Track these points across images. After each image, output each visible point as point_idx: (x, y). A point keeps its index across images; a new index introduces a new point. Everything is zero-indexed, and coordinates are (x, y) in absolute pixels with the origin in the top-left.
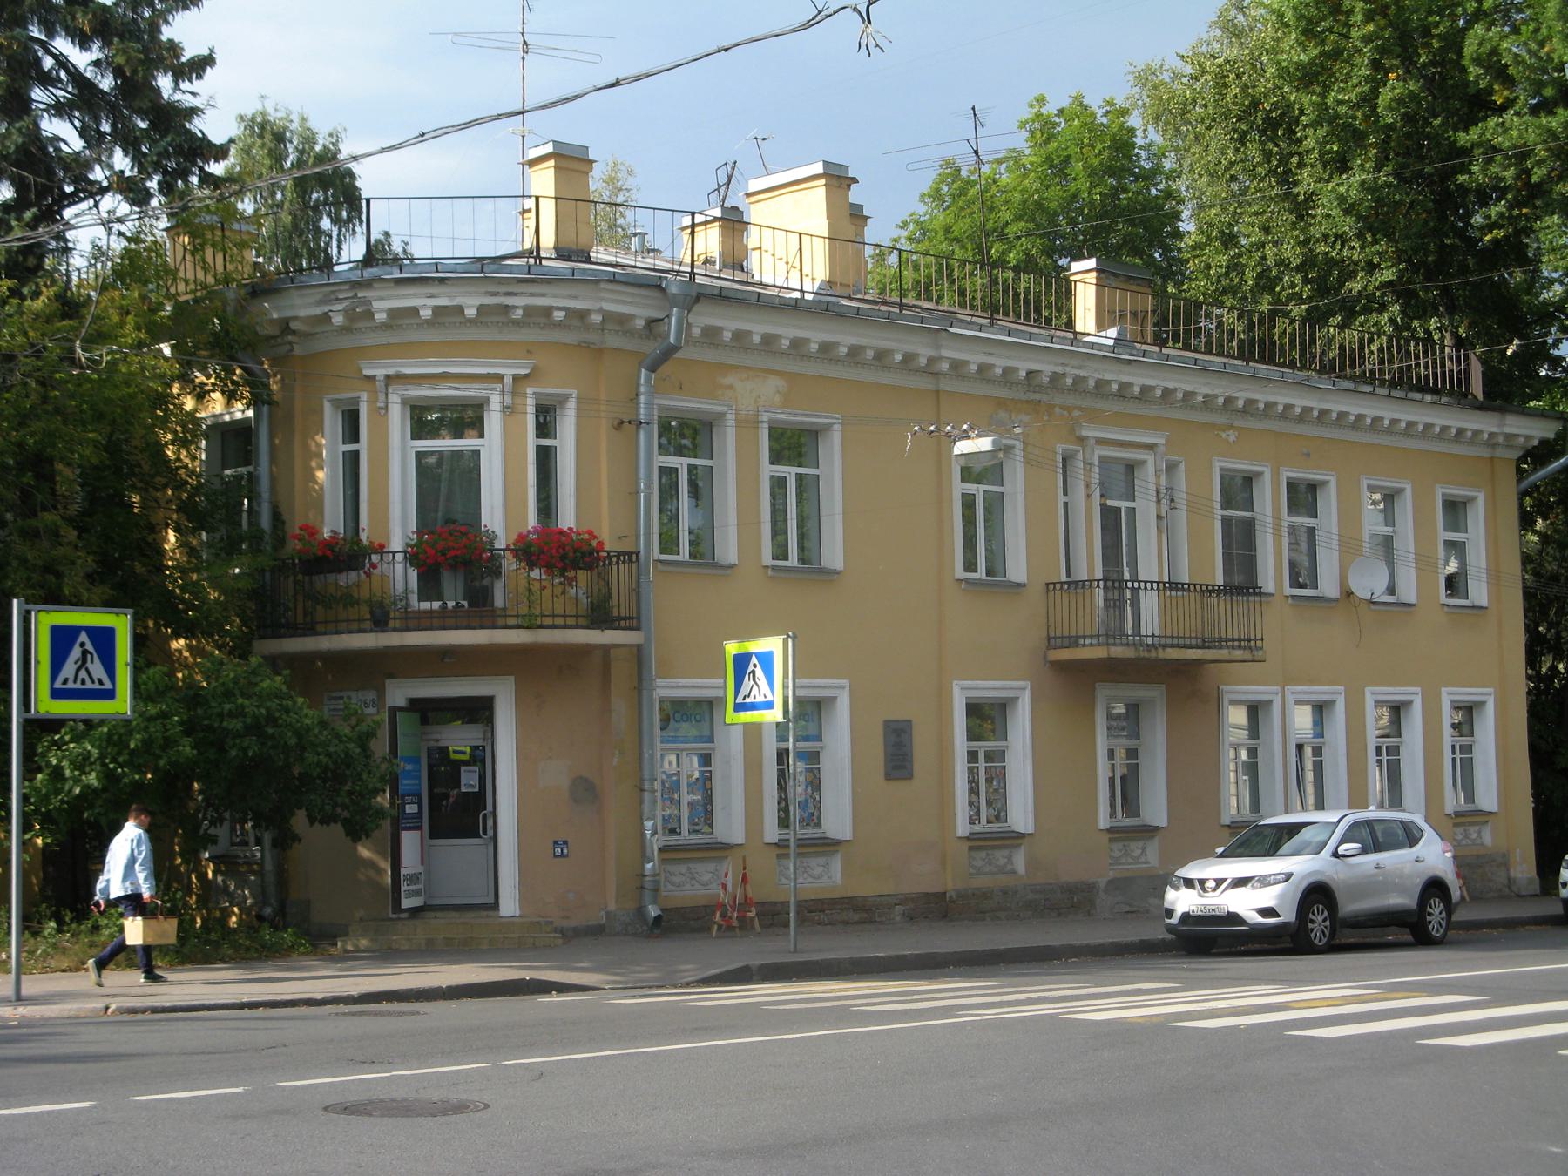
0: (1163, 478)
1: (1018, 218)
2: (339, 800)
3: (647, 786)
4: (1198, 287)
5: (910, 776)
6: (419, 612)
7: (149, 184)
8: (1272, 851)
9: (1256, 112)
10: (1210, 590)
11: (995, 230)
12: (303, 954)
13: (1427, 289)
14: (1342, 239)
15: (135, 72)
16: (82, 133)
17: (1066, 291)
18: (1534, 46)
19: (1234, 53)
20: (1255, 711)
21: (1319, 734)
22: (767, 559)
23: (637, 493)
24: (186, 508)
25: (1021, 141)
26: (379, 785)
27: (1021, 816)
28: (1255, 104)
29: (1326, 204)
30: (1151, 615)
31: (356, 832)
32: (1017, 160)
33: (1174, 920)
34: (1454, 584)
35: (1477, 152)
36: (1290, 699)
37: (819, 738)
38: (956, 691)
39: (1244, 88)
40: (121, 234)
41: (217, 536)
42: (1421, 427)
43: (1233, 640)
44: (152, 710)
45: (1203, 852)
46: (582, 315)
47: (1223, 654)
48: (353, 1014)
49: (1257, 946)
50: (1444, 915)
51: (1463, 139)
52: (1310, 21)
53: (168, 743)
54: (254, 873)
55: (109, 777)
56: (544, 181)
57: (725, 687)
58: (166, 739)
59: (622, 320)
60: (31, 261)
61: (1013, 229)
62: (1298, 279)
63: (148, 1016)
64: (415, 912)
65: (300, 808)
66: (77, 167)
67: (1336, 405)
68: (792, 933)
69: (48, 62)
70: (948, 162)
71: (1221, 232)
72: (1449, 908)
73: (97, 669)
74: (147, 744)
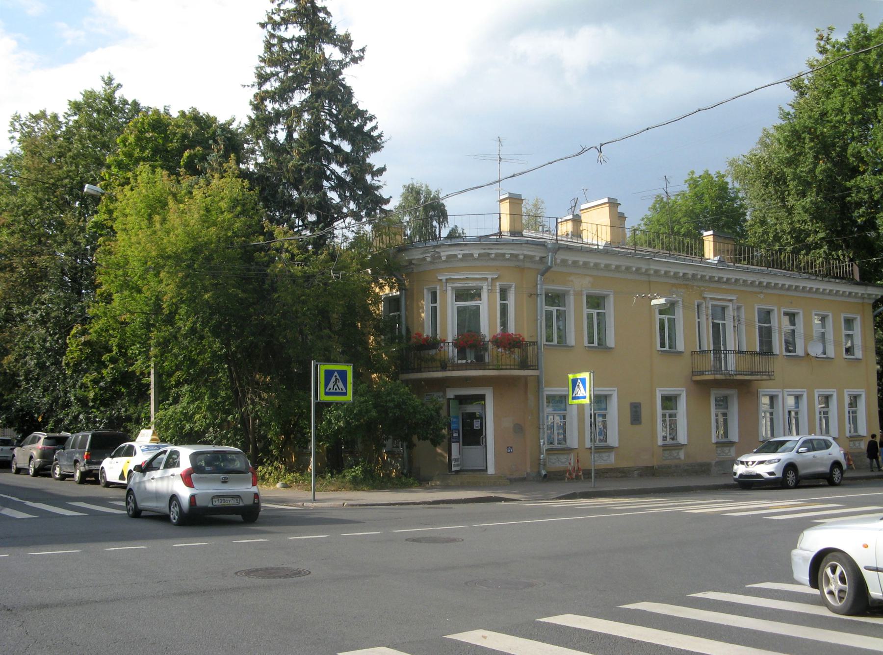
0: (736, 312)
1: (685, 216)
2: (429, 432)
3: (541, 427)
4: (751, 240)
5: (640, 423)
6: (458, 364)
7: (362, 214)
8: (775, 451)
9: (772, 175)
10: (753, 353)
11: (676, 220)
12: (416, 486)
13: (837, 240)
14: (805, 222)
15: (357, 174)
16: (340, 196)
17: (702, 242)
18: (874, 150)
19: (765, 154)
20: (772, 398)
21: (797, 407)
22: (586, 343)
23: (537, 320)
24: (376, 327)
25: (685, 188)
26: (443, 427)
27: (682, 438)
28: (771, 172)
29: (798, 209)
30: (731, 363)
31: (435, 443)
32: (684, 195)
33: (737, 476)
34: (848, 350)
35: (854, 189)
36: (785, 394)
37: (606, 409)
38: (657, 391)
39: (767, 167)
40: (352, 231)
41: (387, 337)
42: (835, 292)
43: (762, 372)
44: (362, 399)
45: (749, 451)
46: (516, 256)
47: (759, 377)
48: (428, 508)
49: (770, 486)
50: (840, 474)
51: (848, 184)
52: (790, 142)
53: (368, 411)
54: (400, 457)
55: (347, 423)
56: (505, 207)
57: (569, 391)
58: (367, 410)
59: (531, 258)
60: (322, 242)
61: (683, 220)
62: (789, 237)
63: (358, 507)
64: (457, 472)
65: (415, 434)
66: (338, 208)
67: (802, 284)
68: (593, 481)
69: (328, 172)
70: (658, 196)
71: (760, 220)
72: (842, 472)
73: (341, 385)
74: (360, 411)
